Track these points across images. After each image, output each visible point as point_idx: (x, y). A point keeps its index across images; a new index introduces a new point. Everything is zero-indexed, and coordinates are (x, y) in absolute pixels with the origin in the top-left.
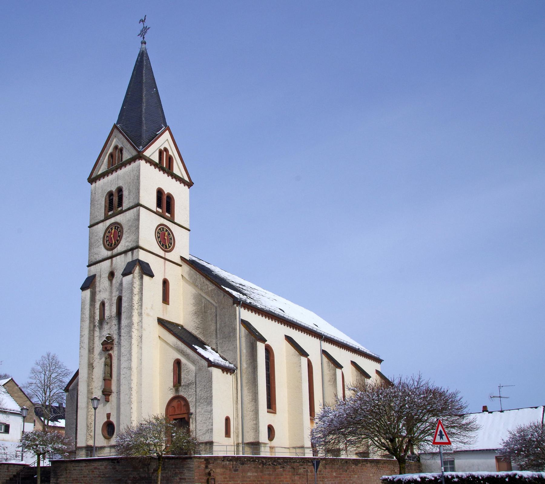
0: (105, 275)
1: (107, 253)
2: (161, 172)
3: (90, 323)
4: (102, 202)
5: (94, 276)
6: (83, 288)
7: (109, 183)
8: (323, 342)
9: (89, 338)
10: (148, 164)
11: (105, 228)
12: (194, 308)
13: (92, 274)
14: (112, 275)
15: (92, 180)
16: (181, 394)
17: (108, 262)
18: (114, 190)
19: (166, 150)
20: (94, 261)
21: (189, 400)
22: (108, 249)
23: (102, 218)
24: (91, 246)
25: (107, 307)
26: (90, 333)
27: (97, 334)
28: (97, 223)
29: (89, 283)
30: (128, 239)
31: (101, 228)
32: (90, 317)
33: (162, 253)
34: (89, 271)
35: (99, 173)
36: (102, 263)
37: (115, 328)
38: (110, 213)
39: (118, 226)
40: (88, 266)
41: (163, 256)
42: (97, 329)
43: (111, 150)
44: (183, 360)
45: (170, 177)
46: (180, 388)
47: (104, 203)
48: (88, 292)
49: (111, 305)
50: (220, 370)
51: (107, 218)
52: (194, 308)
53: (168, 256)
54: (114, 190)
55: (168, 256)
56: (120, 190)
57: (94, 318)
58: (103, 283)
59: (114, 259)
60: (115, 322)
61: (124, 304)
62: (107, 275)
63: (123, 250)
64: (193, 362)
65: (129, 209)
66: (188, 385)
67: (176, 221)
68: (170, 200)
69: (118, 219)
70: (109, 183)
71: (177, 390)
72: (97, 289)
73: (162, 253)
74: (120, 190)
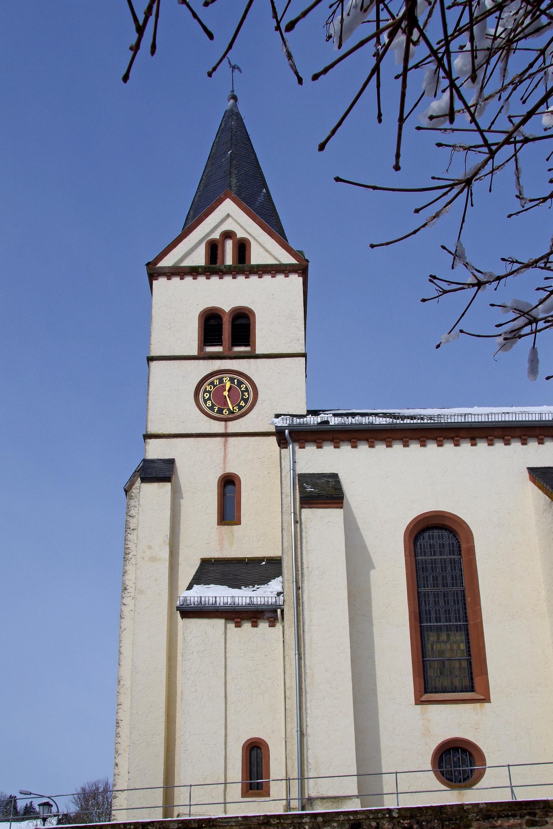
33: (218, 427)
41: (222, 431)
73: (218, 427)
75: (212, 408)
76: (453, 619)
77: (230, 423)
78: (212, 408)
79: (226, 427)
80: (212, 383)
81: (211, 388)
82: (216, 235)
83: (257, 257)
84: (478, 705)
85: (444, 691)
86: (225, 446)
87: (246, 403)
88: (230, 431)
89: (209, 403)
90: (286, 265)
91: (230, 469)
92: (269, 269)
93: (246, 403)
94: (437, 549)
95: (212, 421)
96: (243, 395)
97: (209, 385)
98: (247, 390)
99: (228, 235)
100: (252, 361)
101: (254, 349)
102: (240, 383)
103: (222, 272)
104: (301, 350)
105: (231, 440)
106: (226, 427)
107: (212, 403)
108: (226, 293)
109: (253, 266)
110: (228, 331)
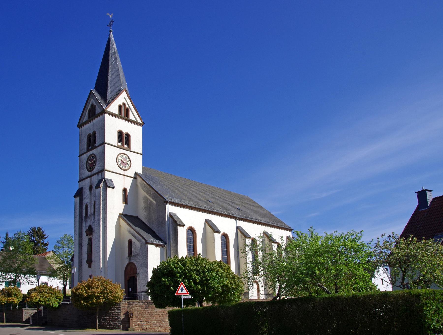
0: (88, 188)
1: (87, 173)
2: (121, 120)
3: (79, 218)
4: (85, 141)
5: (82, 188)
6: (75, 196)
7: (88, 128)
8: (238, 221)
9: (79, 228)
10: (111, 116)
11: (87, 158)
12: (144, 205)
13: (81, 187)
14: (91, 188)
15: (80, 126)
16: (133, 261)
17: (89, 179)
18: (91, 133)
19: (124, 104)
20: (82, 178)
21: (136, 265)
22: (89, 171)
23: (86, 151)
24: (80, 168)
25: (89, 209)
26: (79, 225)
27: (84, 225)
28: (83, 154)
29: (79, 193)
30: (99, 165)
31: (85, 157)
32: (79, 215)
33: (122, 172)
34: (79, 185)
35: (84, 121)
36: (86, 180)
37: (93, 221)
38: (90, 147)
39: (93, 157)
40: (78, 182)
41: (123, 174)
42: (84, 222)
43: (89, 107)
44: (134, 240)
45: (127, 122)
46: (132, 258)
47: (86, 141)
48: (78, 199)
49: (91, 207)
50: (154, 246)
51: (88, 150)
52: (144, 205)
53: (126, 173)
54: (91, 133)
55: (126, 173)
56: (94, 133)
57: (82, 215)
58: (87, 193)
59: (92, 177)
60: (93, 217)
61: (97, 207)
62: (89, 188)
63: (97, 171)
64: (139, 240)
65: (99, 146)
66: (136, 256)
67: (132, 150)
68: (128, 136)
69: (94, 151)
70: (88, 128)
71: (130, 259)
72: (84, 197)
73: (122, 172)
74: (94, 133)
83: (131, 117)
99: (124, 104)
102: (127, 159)
103: (122, 119)
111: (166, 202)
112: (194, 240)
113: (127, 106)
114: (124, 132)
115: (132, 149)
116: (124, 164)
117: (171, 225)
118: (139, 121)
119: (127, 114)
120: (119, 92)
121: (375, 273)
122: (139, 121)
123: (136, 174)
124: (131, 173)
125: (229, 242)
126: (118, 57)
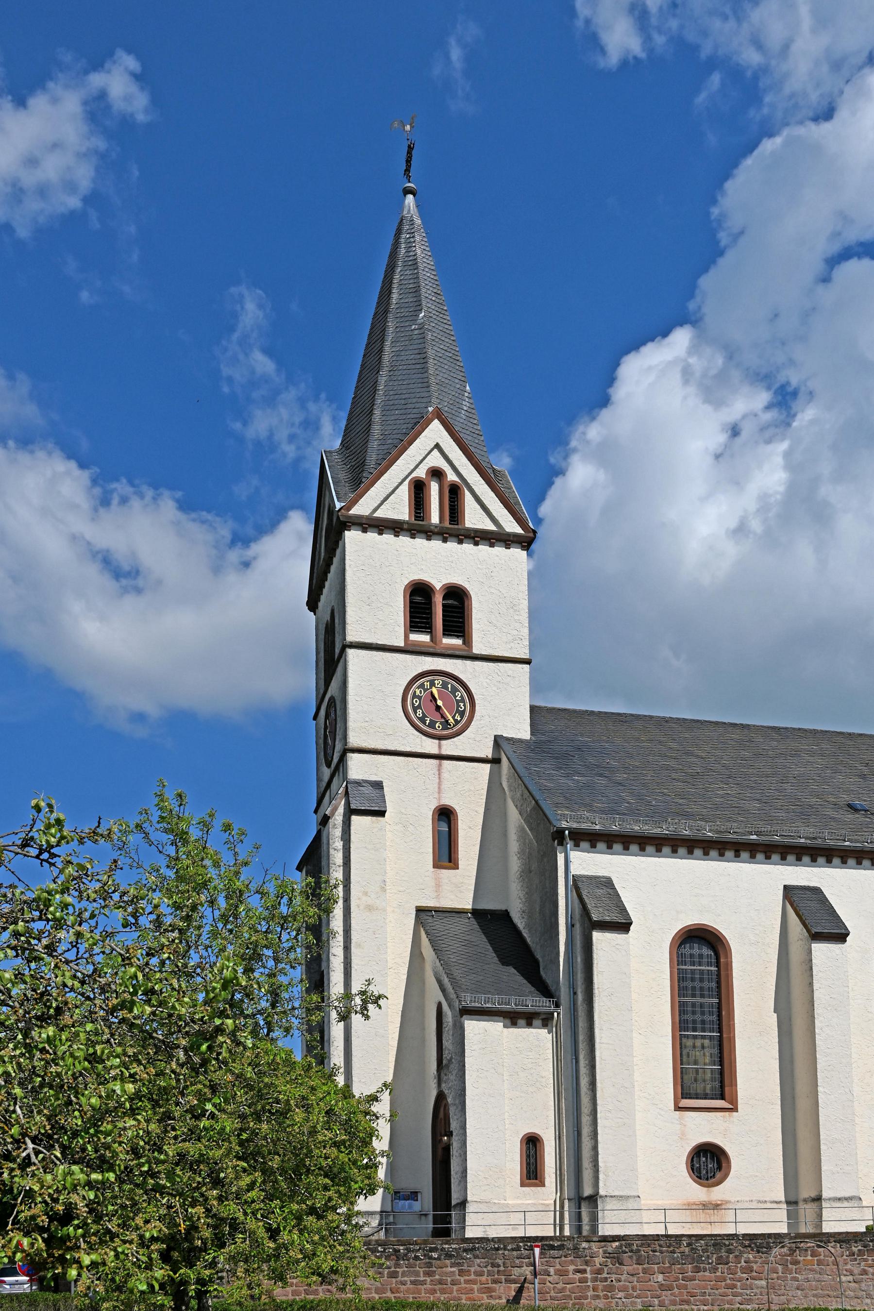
33: (430, 746)
41: (434, 751)
73: (430, 746)
75: (422, 720)
76: (709, 1072)
77: (444, 742)
78: (422, 720)
79: (440, 747)
80: (422, 686)
81: (421, 692)
82: (421, 473)
83: (473, 518)
84: (727, 1114)
85: (697, 1097)
86: (439, 770)
87: (462, 717)
88: (444, 752)
89: (419, 713)
90: (509, 534)
91: (447, 801)
92: (489, 536)
93: (462, 717)
94: (698, 1009)
95: (424, 738)
96: (458, 706)
97: (418, 688)
98: (463, 700)
99: (436, 473)
100: (468, 663)
101: (468, 642)
102: (454, 690)
103: (429, 533)
104: (524, 654)
105: (446, 763)
106: (440, 747)
107: (423, 713)
108: (441, 563)
109: (469, 530)
110: (435, 612)
111: (559, 836)
112: (719, 983)
113: (451, 477)
114: (438, 584)
115: (478, 648)
116: (440, 711)
117: (578, 926)
118: (512, 526)
119: (454, 509)
120: (418, 426)
121: (374, 1138)
122: (512, 526)
123: (498, 741)
124: (476, 741)
125: (729, 976)
126: (426, 292)
